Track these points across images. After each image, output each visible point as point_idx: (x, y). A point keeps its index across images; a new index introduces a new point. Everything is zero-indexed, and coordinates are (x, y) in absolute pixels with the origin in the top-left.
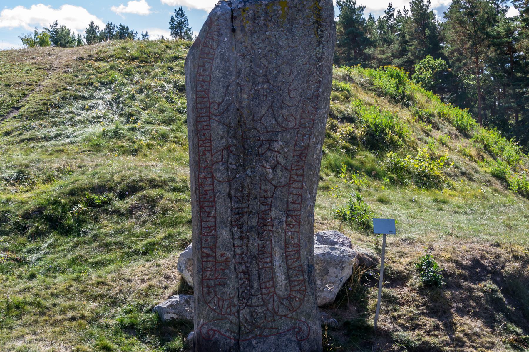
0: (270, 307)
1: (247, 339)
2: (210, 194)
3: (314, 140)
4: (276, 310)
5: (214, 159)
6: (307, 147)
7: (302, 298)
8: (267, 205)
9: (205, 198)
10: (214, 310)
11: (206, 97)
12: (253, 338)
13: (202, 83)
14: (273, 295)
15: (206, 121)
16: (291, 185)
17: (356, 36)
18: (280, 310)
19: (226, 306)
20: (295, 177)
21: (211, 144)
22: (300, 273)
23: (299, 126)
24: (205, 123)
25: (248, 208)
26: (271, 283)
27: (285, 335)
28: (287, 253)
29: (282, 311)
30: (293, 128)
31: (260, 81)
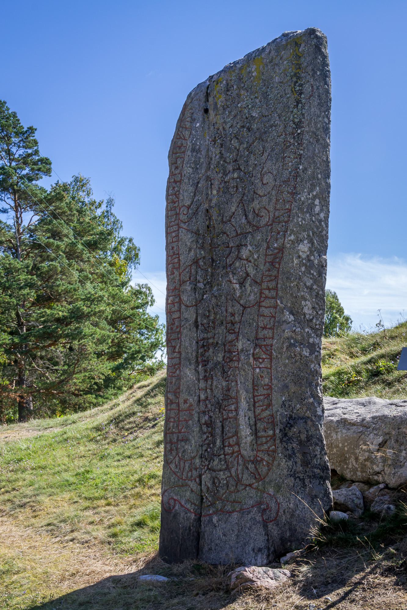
0: (233, 471)
6: (281, 249)
14: (238, 456)
23: (273, 221)
29: (246, 478)
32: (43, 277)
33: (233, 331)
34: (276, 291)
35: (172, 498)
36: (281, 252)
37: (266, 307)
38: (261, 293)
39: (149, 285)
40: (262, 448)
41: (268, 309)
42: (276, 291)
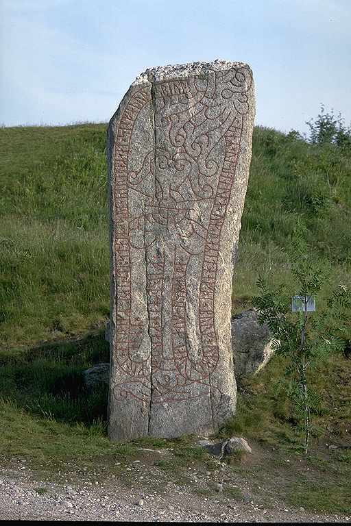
1: (158, 402)
3: (231, 210)
24: (122, 192)
29: (194, 375)
35: (124, 390)
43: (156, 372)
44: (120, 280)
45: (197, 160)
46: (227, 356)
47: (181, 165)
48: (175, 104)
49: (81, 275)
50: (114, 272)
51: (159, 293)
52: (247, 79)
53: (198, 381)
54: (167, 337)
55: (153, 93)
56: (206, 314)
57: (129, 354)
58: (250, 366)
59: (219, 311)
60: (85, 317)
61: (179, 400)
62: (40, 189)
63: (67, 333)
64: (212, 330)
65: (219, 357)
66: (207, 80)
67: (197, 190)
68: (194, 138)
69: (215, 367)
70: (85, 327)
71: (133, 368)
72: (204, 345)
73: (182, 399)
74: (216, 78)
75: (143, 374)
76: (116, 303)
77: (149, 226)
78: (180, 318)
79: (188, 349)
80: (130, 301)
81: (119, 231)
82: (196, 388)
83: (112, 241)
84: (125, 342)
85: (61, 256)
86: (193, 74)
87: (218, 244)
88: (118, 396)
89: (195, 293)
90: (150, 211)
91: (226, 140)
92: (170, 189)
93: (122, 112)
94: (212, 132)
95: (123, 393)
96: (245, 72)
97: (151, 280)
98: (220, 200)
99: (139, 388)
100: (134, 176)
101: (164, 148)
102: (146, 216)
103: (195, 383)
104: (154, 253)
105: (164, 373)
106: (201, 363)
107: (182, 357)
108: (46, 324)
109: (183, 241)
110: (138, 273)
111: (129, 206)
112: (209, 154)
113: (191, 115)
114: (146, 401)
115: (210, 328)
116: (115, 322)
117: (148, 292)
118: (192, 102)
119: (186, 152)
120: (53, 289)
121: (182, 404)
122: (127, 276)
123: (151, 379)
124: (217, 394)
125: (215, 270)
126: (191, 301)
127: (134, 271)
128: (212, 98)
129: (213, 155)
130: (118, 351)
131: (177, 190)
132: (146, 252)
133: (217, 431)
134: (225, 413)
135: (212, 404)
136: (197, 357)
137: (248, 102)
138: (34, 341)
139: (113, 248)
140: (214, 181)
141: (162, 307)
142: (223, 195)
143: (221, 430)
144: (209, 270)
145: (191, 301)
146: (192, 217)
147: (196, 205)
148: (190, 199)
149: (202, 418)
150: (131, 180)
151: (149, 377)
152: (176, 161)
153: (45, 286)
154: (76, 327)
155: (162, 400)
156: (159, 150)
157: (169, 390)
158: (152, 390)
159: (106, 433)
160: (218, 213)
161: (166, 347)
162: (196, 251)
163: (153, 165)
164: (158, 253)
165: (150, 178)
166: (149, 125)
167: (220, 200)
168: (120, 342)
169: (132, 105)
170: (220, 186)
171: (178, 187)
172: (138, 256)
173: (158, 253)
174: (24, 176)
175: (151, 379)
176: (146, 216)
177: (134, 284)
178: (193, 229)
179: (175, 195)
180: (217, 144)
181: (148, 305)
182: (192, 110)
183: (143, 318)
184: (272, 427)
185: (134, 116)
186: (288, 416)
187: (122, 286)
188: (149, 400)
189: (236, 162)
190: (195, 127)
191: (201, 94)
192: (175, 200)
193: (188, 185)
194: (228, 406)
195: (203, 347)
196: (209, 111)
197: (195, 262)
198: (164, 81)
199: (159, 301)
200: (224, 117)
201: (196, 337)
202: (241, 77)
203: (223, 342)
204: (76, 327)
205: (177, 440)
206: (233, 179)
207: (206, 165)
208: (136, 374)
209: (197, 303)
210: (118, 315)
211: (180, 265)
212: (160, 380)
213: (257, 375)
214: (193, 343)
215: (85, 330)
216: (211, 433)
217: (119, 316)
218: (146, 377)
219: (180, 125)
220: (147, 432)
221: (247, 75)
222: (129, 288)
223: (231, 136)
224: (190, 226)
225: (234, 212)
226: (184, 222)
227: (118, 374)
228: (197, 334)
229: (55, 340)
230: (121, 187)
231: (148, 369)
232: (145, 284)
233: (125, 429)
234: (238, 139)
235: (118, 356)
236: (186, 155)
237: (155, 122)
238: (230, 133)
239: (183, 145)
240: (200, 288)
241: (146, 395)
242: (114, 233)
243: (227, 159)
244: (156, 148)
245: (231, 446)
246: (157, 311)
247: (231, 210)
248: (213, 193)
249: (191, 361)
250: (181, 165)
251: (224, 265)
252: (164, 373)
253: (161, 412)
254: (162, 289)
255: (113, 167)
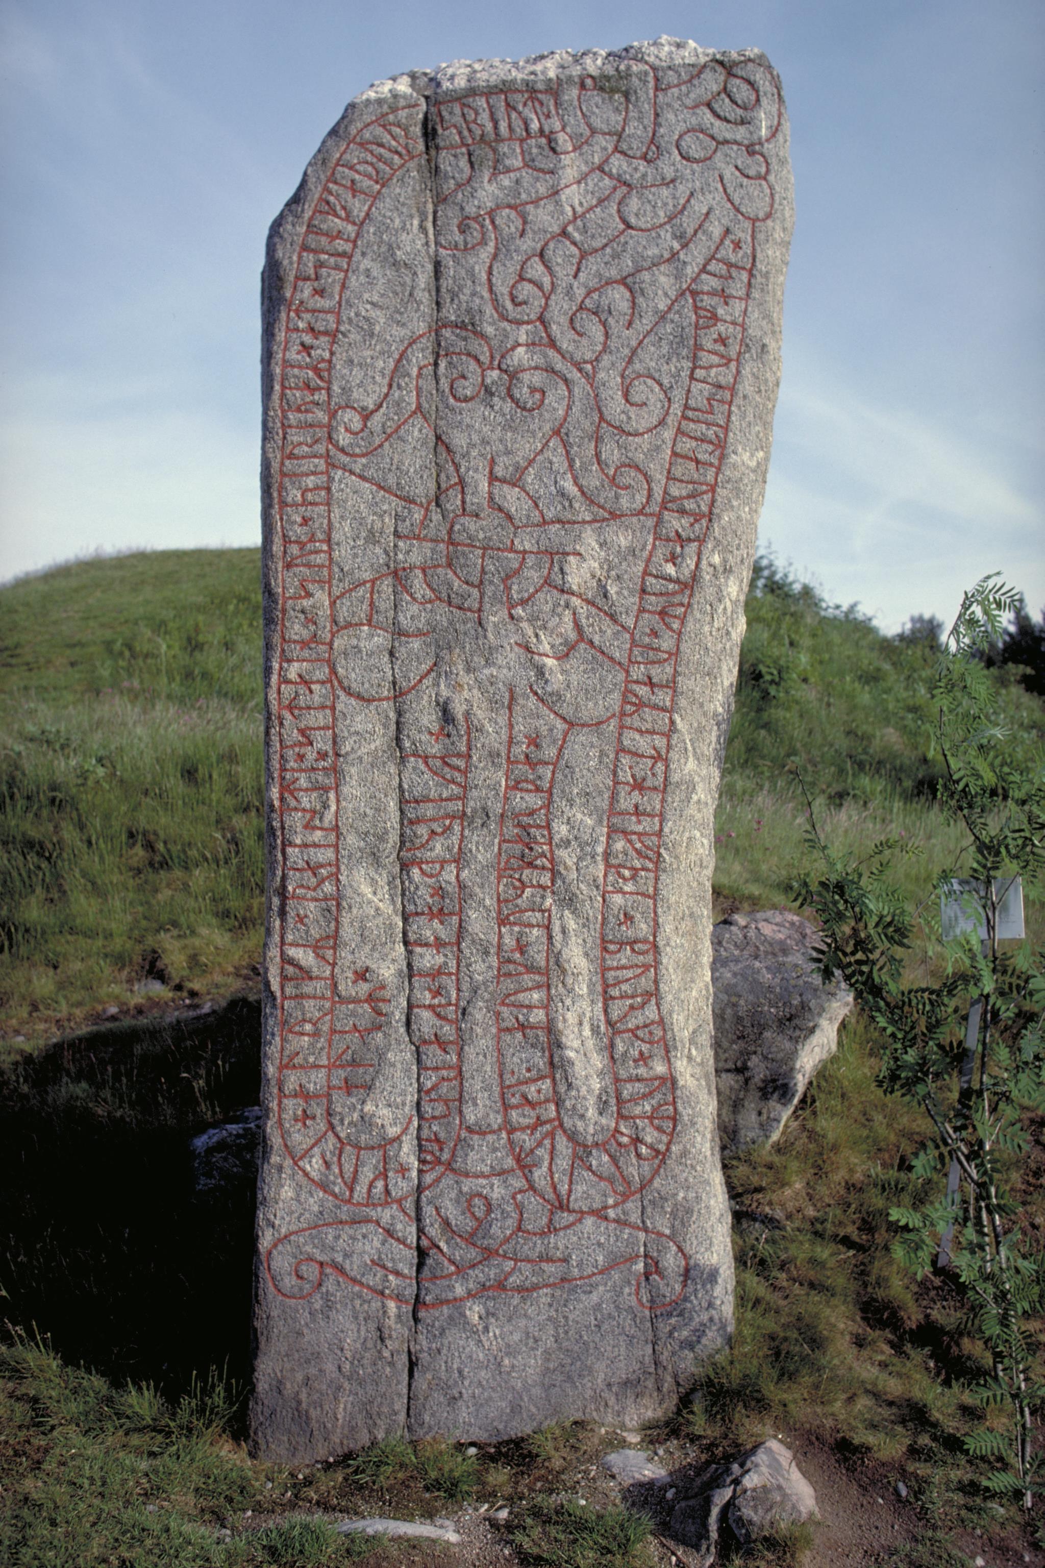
0: (539, 1175)
1: (448, 1302)
2: (322, 742)
3: (716, 559)
4: (564, 1189)
5: (343, 614)
6: (691, 584)
7: (662, 1147)
8: (538, 789)
9: (301, 757)
10: (324, 1186)
11: (319, 389)
12: (470, 1295)
13: (308, 339)
14: (552, 1135)
15: (314, 473)
16: (628, 721)
17: (510, 1527)
18: (579, 1189)
19: (367, 1174)
20: (642, 691)
21: (331, 559)
22: (659, 1050)
23: (664, 506)
24: (310, 481)
25: (463, 798)
26: (546, 1085)
27: (594, 1286)
28: (611, 974)
29: (585, 1191)
30: (641, 512)
31: (523, 339)
32: (506, 1455)
33: (530, 787)
34: (670, 692)
35: (311, 1259)
36: (688, 592)
37: (640, 732)
38: (627, 692)
39: (617, 48)
40: (638, 1110)
41: (648, 738)
42: (670, 692)
43: (438, 1180)
44: (296, 820)
45: (588, 369)
46: (702, 1106)
47: (533, 390)
48: (508, 170)
49: (239, 821)
50: (275, 793)
51: (449, 874)
52: (764, 101)
53: (600, 1214)
54: (480, 1054)
55: (429, 133)
56: (628, 951)
57: (329, 1113)
58: (754, 1117)
59: (676, 940)
60: (234, 940)
61: (525, 1291)
62: (193, 645)
63: (179, 988)
64: (651, 1012)
65: (675, 1119)
66: (626, 95)
67: (593, 480)
68: (580, 293)
69: (661, 1156)
70: (231, 969)
71: (348, 1168)
72: (623, 1074)
73: (536, 1287)
74: (657, 89)
75: (387, 1192)
76: (283, 913)
77: (412, 615)
78: (531, 969)
79: (562, 1088)
80: (335, 905)
81: (297, 630)
82: (588, 1242)
83: (268, 671)
84: (316, 1066)
85: (190, 773)
86: (576, 71)
87: (672, 685)
88: (289, 1282)
89: (582, 870)
90: (415, 558)
91: (696, 308)
92: (493, 478)
93: (316, 192)
94: (646, 276)
95: (311, 1271)
96: (759, 77)
97: (418, 821)
98: (675, 523)
99: (371, 1245)
100: (357, 425)
101: (469, 326)
102: (399, 576)
103: (589, 1221)
104: (429, 719)
105: (468, 1185)
106: (608, 1143)
107: (539, 1122)
108: (120, 960)
109: (540, 671)
110: (366, 794)
111: (336, 536)
112: (634, 352)
113: (568, 210)
114: (399, 1298)
115: (643, 1006)
116: (275, 986)
117: (405, 866)
118: (571, 166)
119: (552, 344)
120: (157, 858)
121: (540, 1305)
122: (326, 806)
123: (418, 1208)
124: (671, 1261)
125: (658, 783)
126: (569, 901)
127: (352, 788)
128: (644, 157)
129: (649, 359)
130: (289, 1103)
131: (516, 482)
132: (399, 714)
133: (672, 1403)
134: (700, 1333)
135: (652, 1301)
136: (592, 1121)
137: (771, 178)
138: (78, 1013)
139: (273, 695)
140: (654, 451)
141: (461, 930)
142: (690, 505)
143: (685, 1401)
144: (639, 785)
145: (569, 901)
146: (574, 581)
147: (589, 539)
148: (568, 516)
149: (618, 1357)
150: (343, 438)
151: (409, 1204)
152: (513, 375)
153: (139, 852)
154: (204, 970)
155: (459, 1290)
156: (451, 333)
157: (489, 1253)
158: (422, 1254)
159: (240, 1429)
160: (670, 569)
161: (474, 1085)
162: (591, 710)
163: (428, 385)
164: (447, 716)
165: (418, 432)
166: (413, 242)
167: (675, 523)
168: (295, 1059)
169: (351, 168)
170: (678, 472)
171: (521, 471)
172: (366, 730)
173: (447, 716)
174: (163, 623)
175: (418, 1208)
176: (399, 576)
177: (351, 840)
178: (578, 626)
179: (511, 498)
180: (663, 318)
181: (405, 919)
182: (574, 196)
183: (388, 971)
184: (868, 1372)
185: (359, 208)
186: (913, 1317)
187: (304, 844)
188: (410, 1292)
189: (733, 389)
190: (583, 255)
191: (608, 143)
192: (510, 517)
193: (559, 462)
194: (710, 1305)
195: (617, 1080)
196: (634, 203)
197: (586, 753)
198: (472, 92)
199: (448, 906)
200: (688, 223)
201: (590, 1043)
202: (743, 92)
203: (690, 1058)
204: (204, 970)
205: (515, 1453)
206: (721, 446)
207: (626, 395)
208: (361, 1190)
209: (592, 909)
210: (287, 960)
211: (531, 764)
212: (452, 1212)
213: (779, 1149)
214: (579, 1070)
215: (230, 980)
216: (650, 1414)
217: (291, 962)
218: (399, 1201)
219: (528, 244)
220: (402, 1417)
221: (765, 86)
222: (330, 854)
223: (713, 293)
224: (568, 616)
225: (728, 571)
226: (546, 600)
227: (287, 1192)
228: (595, 1030)
229: (140, 1011)
230: (307, 465)
231: (403, 1170)
232: (393, 838)
233: (314, 1413)
234: (738, 307)
235: (288, 1126)
236: (551, 353)
237: (437, 234)
238: (712, 283)
239: (541, 319)
240: (607, 855)
241: (397, 1273)
242: (276, 639)
243: (699, 373)
244: (438, 327)
245: (747, 1512)
246: (439, 944)
247: (716, 559)
248: (649, 496)
249: (572, 1137)
250: (533, 390)
251: (691, 764)
252: (468, 1185)
253: (455, 1336)
254: (460, 859)
255: (277, 387)
